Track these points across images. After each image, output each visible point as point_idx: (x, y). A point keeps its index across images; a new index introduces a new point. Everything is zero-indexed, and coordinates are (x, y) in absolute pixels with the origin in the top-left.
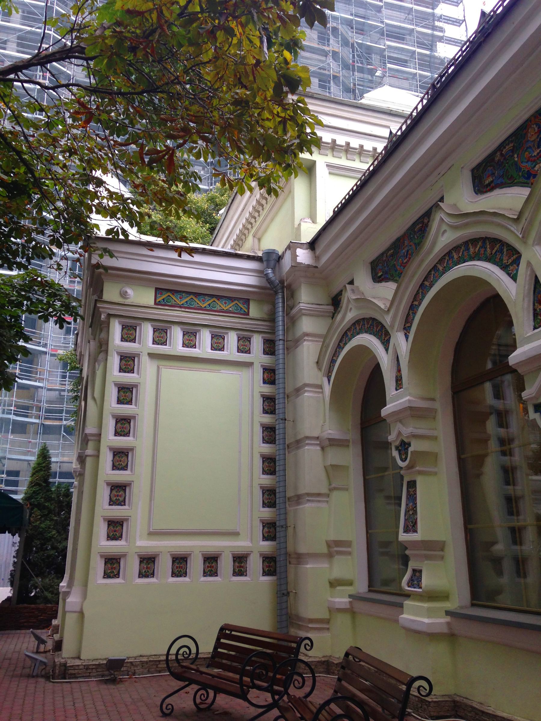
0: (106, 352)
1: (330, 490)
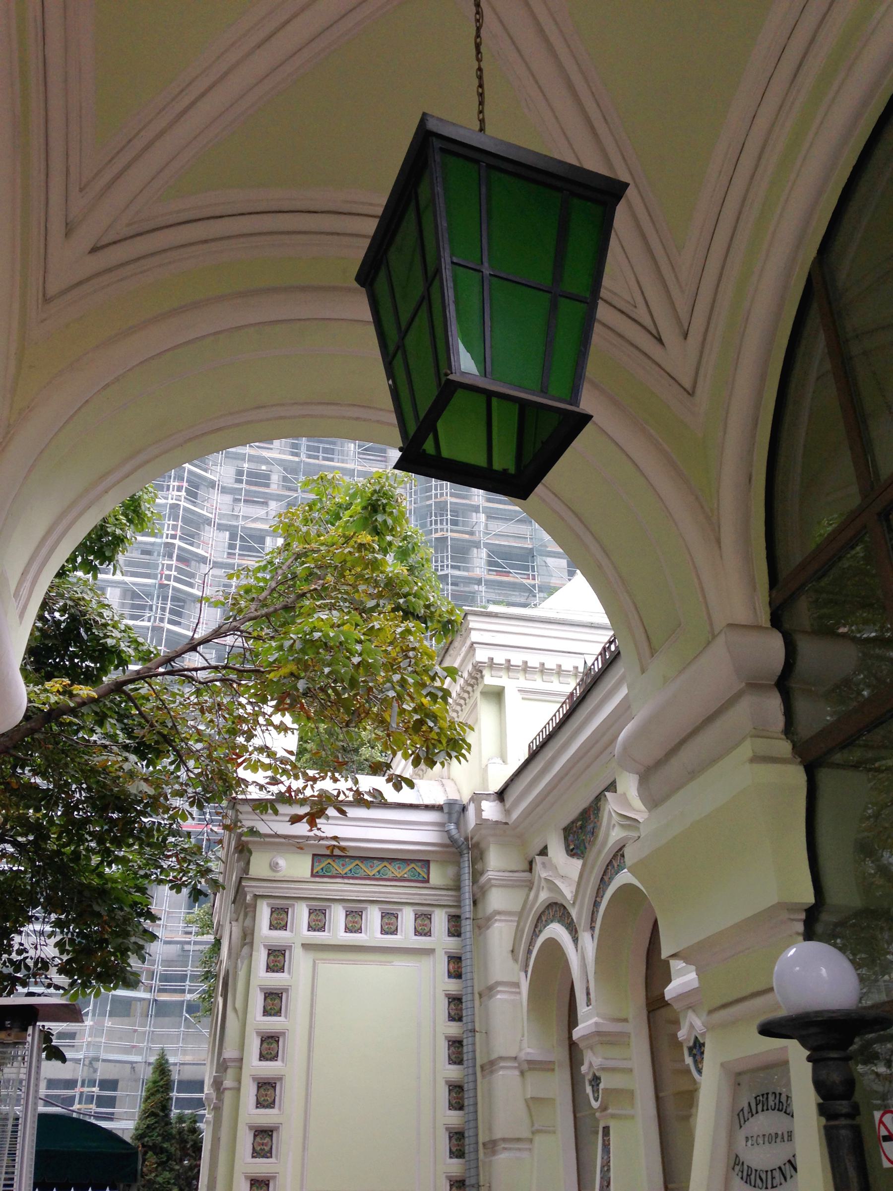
0: (251, 944)
1: (533, 1133)
